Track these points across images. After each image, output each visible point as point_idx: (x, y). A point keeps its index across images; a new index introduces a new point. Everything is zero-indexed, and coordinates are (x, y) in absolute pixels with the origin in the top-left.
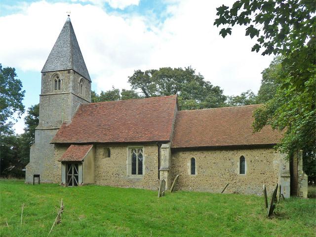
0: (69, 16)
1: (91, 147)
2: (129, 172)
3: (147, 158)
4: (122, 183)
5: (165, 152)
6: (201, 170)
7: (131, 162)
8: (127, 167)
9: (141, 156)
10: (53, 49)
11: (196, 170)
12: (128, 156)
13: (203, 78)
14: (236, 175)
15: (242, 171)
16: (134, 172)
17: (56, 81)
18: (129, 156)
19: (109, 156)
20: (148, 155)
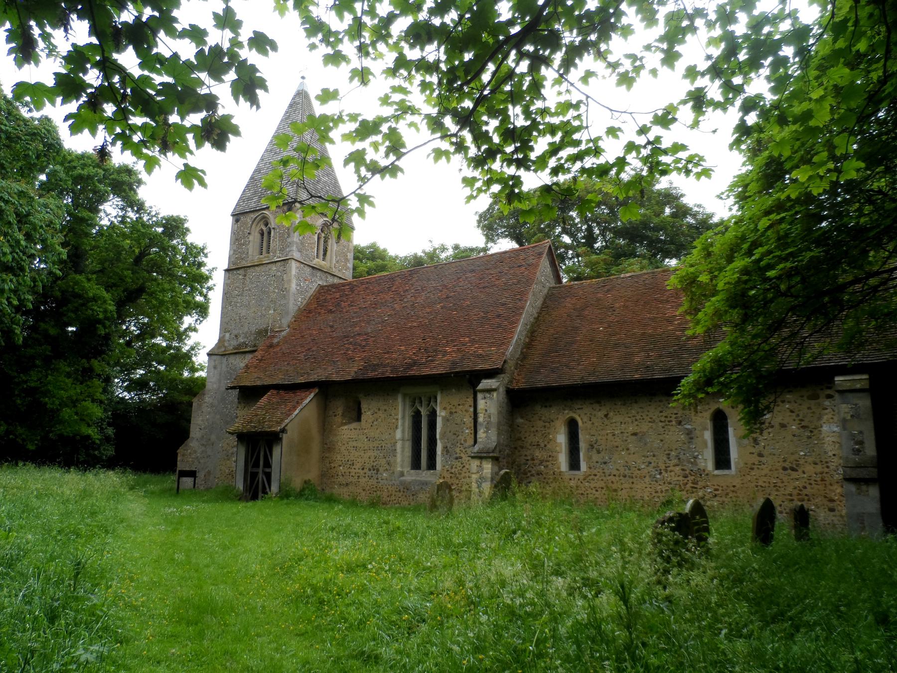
0: (303, 78)
1: (309, 397)
2: (403, 461)
3: (446, 420)
4: (385, 494)
5: (490, 405)
6: (596, 457)
7: (408, 434)
8: (399, 450)
9: (433, 415)
10: (262, 160)
11: (581, 455)
12: (400, 416)
13: (682, 195)
14: (701, 472)
15: (722, 460)
16: (416, 464)
17: (262, 234)
18: (403, 417)
19: (359, 419)
20: (446, 409)
